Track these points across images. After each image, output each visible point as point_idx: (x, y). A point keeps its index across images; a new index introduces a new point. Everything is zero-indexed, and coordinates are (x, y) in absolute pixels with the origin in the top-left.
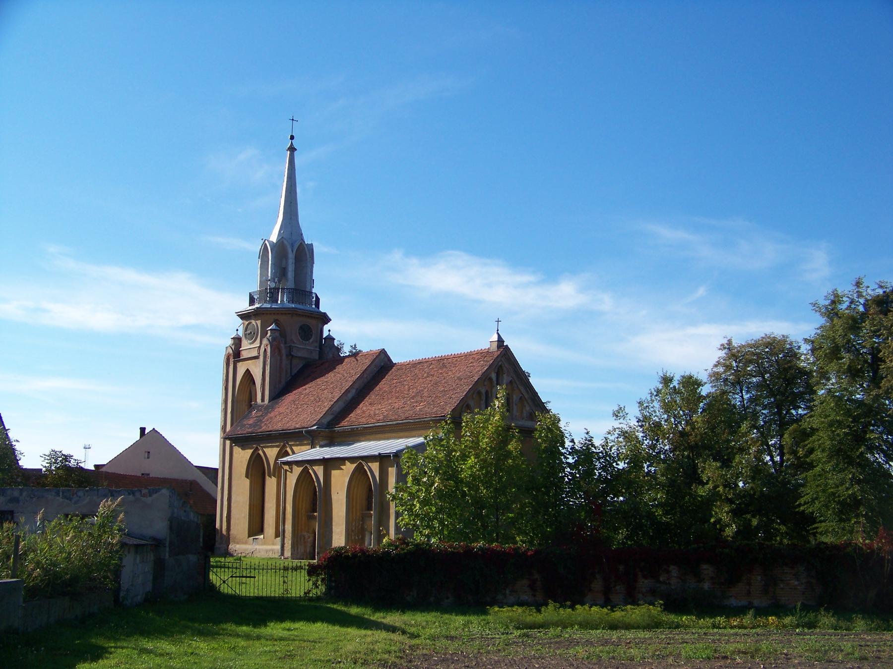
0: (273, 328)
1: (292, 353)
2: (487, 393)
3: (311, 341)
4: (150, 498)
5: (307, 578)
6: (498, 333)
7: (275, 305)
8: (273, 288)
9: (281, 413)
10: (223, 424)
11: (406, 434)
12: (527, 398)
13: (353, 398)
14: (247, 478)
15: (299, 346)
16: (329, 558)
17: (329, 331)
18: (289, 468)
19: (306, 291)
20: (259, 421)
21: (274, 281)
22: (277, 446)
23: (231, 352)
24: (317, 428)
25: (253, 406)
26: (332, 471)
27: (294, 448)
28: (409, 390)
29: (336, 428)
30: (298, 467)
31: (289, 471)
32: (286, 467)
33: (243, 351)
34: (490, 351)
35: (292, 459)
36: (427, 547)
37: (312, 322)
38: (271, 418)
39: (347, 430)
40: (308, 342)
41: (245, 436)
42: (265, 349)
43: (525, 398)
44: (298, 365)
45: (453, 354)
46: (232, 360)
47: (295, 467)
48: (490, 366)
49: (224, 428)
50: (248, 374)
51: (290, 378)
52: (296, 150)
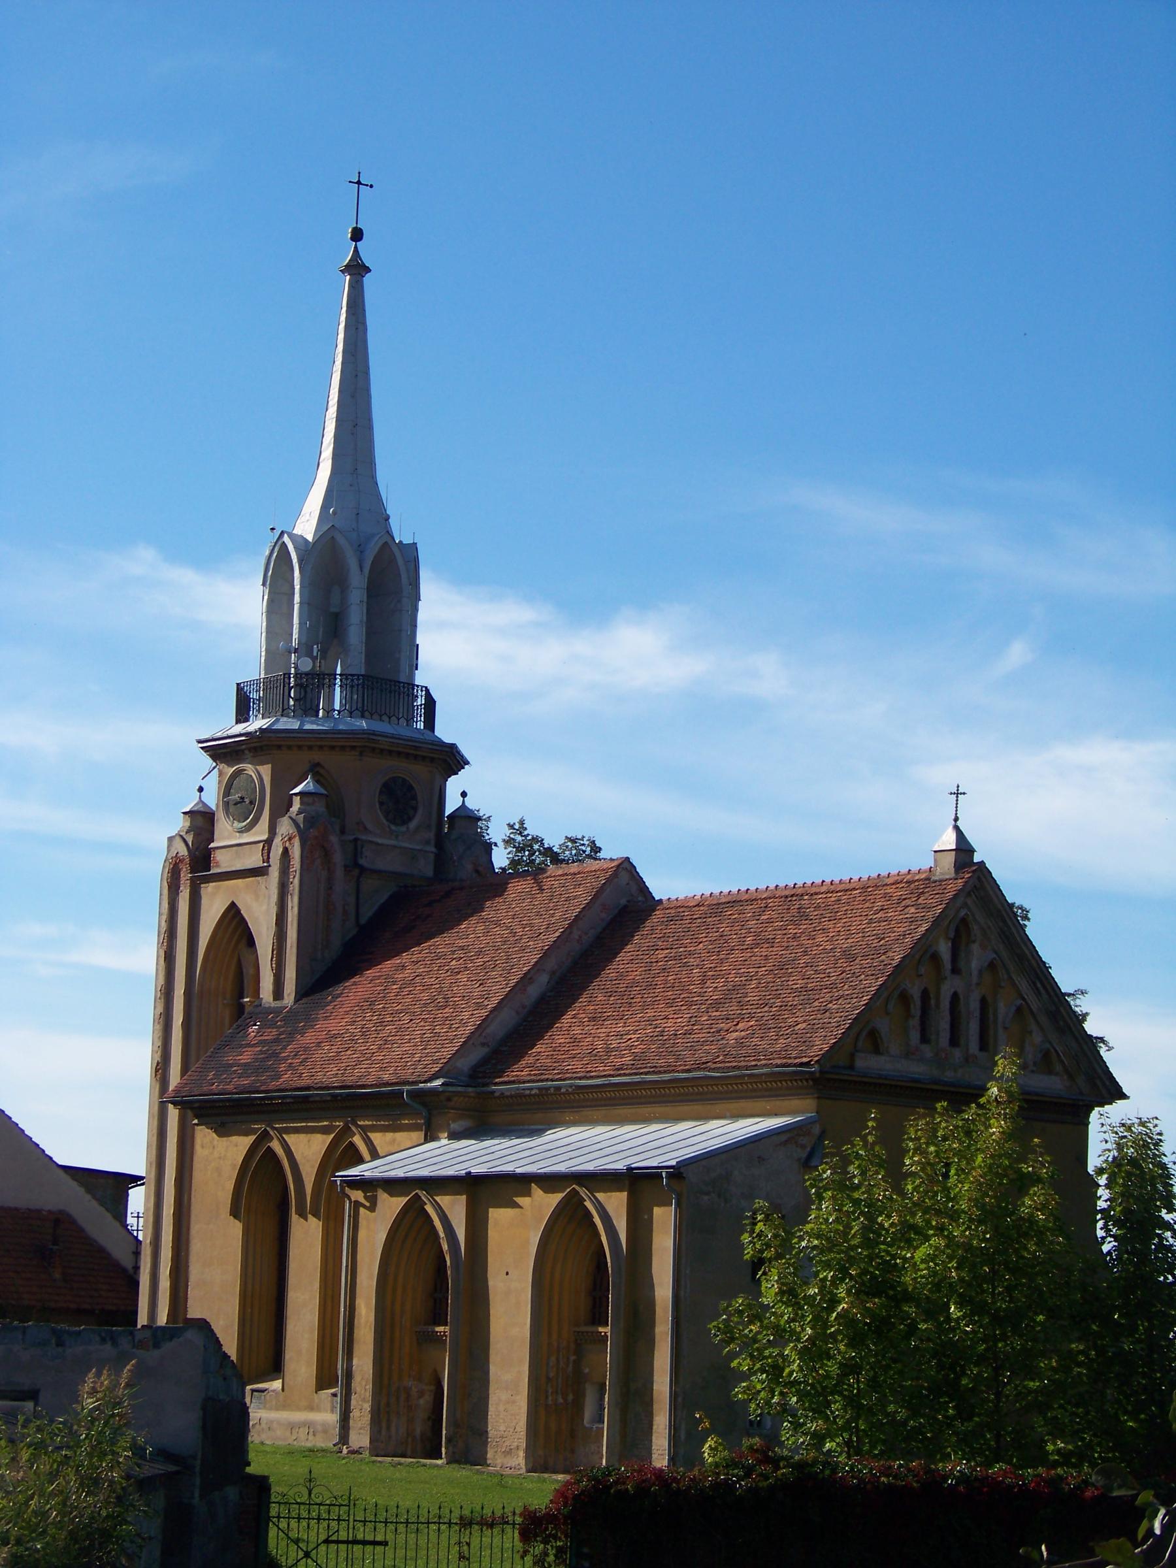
0: (307, 790)
1: (362, 861)
2: (925, 994)
3: (413, 824)
4: (156, 1353)
5: (519, 1545)
6: (957, 828)
7: (312, 723)
8: (307, 674)
9: (335, 1036)
10: (158, 1058)
11: (698, 1108)
12: (1035, 1010)
13: (542, 1000)
14: (235, 1217)
15: (380, 841)
16: (575, 1497)
17: (464, 794)
18: (366, 1197)
19: (400, 682)
20: (270, 1057)
21: (309, 654)
22: (325, 1131)
23: (183, 851)
24: (443, 1084)
25: (247, 1009)
26: (491, 1210)
27: (376, 1137)
28: (703, 982)
29: (496, 1084)
30: (391, 1195)
31: (364, 1206)
32: (357, 1195)
33: (218, 852)
34: (934, 878)
35: (376, 1174)
36: (827, 1472)
37: (416, 772)
38: (306, 1049)
39: (528, 1092)
40: (403, 829)
41: (229, 1100)
42: (286, 851)
43: (1031, 1010)
44: (377, 895)
45: (828, 880)
46: (185, 876)
47: (383, 1196)
48: (937, 922)
49: (161, 1070)
50: (233, 916)
51: (354, 932)
52: (368, 270)
